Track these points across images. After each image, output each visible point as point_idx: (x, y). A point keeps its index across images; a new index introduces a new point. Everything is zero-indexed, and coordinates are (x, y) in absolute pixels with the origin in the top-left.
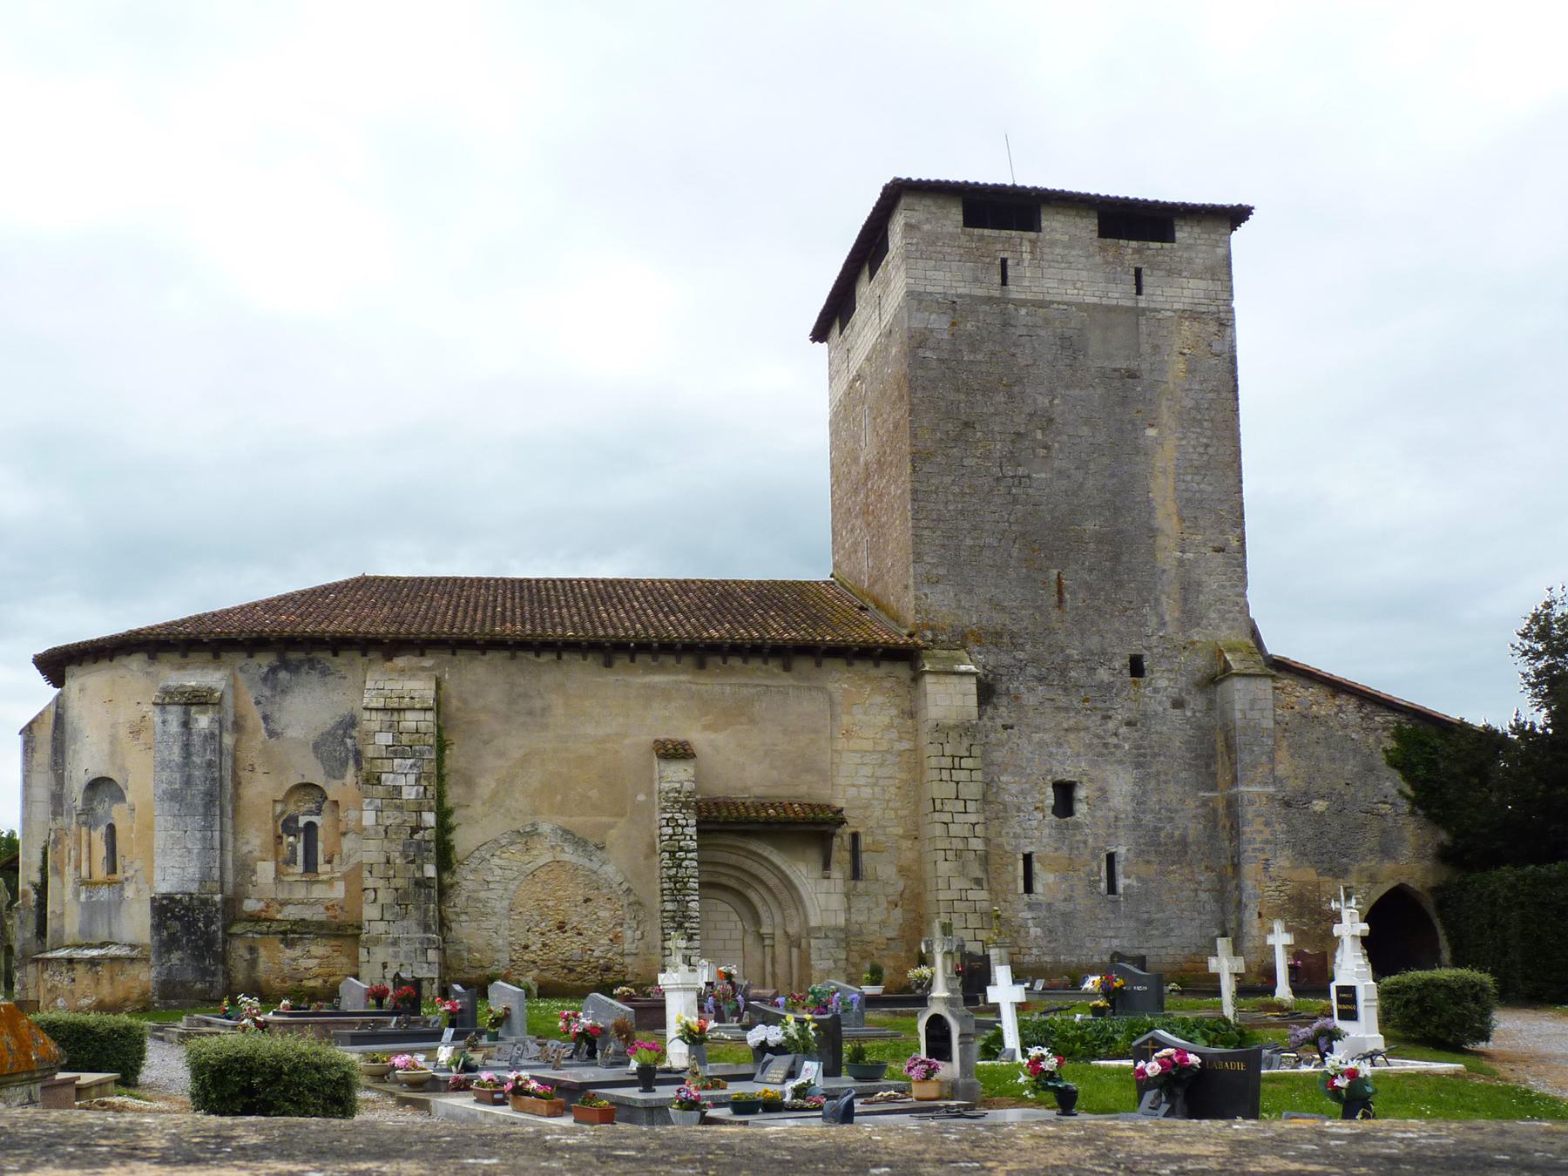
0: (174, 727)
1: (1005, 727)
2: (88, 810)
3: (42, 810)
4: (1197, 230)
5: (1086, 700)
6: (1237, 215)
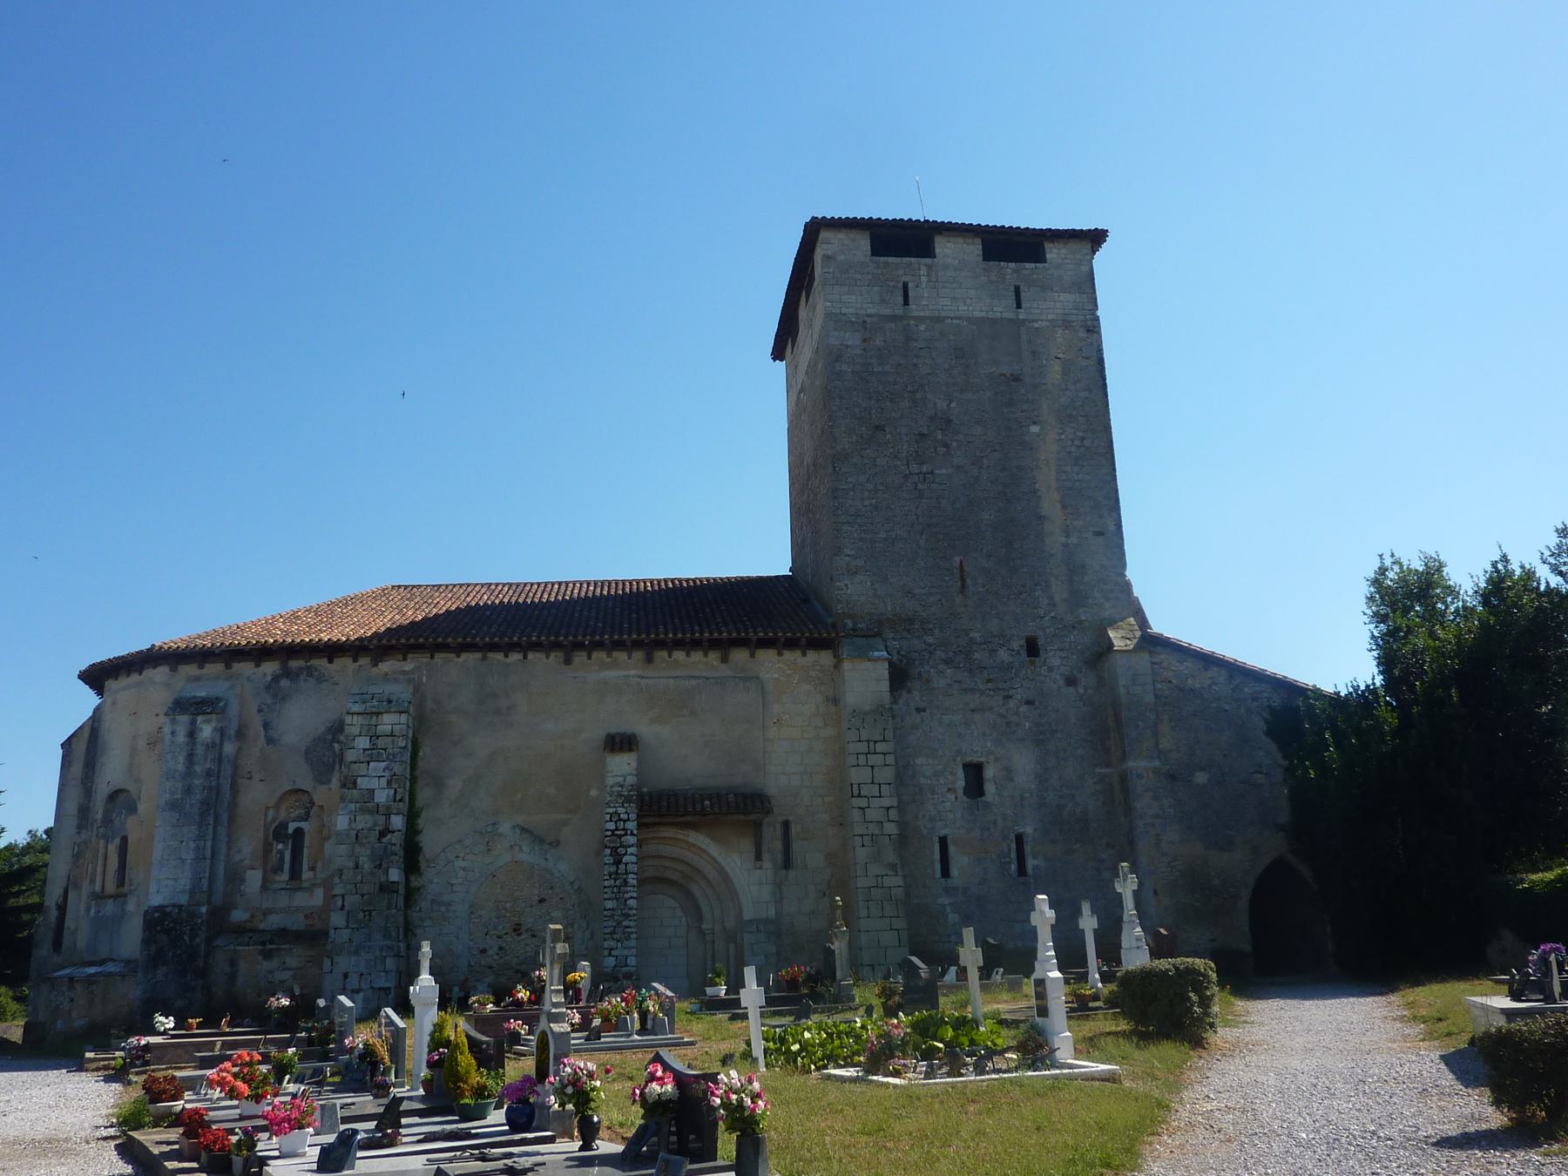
0: (181, 738)
1: (919, 710)
2: (107, 821)
3: (71, 822)
4: (1064, 251)
5: (989, 681)
6: (1096, 238)
